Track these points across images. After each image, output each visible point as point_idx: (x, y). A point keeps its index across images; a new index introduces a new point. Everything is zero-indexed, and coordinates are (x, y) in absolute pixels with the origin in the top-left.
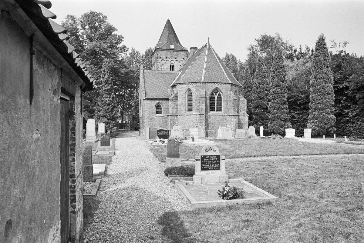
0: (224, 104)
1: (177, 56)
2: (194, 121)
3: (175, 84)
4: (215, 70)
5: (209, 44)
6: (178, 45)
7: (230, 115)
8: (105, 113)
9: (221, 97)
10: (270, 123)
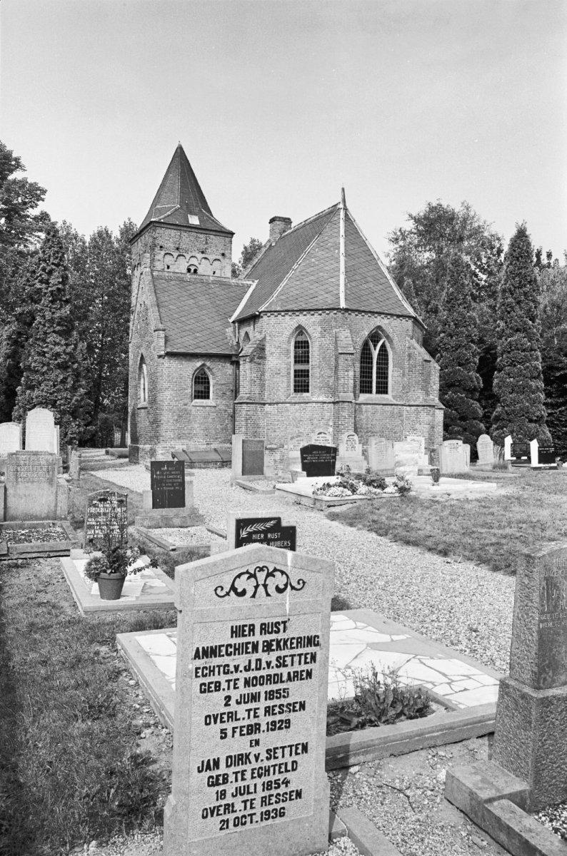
0: (396, 374)
1: (206, 246)
2: (315, 422)
3: (257, 313)
4: (369, 279)
5: (345, 205)
6: (207, 216)
7: (412, 403)
8: (54, 392)
9: (387, 355)
10: (497, 429)
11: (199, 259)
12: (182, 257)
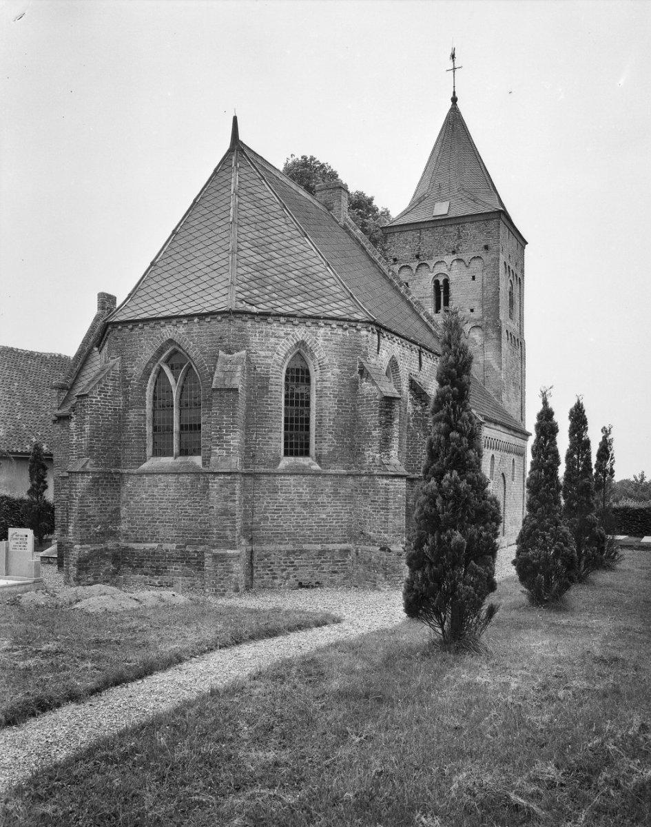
12: (424, 268)
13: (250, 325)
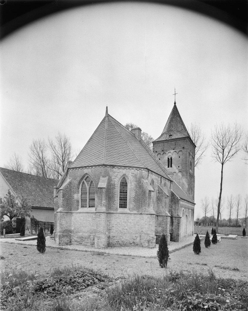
11: (172, 152)
13: (109, 169)
